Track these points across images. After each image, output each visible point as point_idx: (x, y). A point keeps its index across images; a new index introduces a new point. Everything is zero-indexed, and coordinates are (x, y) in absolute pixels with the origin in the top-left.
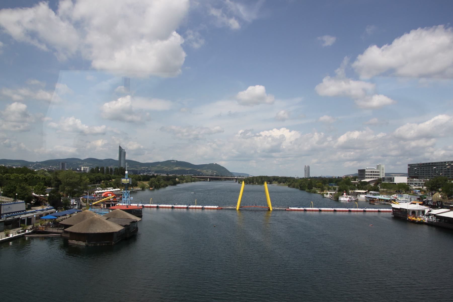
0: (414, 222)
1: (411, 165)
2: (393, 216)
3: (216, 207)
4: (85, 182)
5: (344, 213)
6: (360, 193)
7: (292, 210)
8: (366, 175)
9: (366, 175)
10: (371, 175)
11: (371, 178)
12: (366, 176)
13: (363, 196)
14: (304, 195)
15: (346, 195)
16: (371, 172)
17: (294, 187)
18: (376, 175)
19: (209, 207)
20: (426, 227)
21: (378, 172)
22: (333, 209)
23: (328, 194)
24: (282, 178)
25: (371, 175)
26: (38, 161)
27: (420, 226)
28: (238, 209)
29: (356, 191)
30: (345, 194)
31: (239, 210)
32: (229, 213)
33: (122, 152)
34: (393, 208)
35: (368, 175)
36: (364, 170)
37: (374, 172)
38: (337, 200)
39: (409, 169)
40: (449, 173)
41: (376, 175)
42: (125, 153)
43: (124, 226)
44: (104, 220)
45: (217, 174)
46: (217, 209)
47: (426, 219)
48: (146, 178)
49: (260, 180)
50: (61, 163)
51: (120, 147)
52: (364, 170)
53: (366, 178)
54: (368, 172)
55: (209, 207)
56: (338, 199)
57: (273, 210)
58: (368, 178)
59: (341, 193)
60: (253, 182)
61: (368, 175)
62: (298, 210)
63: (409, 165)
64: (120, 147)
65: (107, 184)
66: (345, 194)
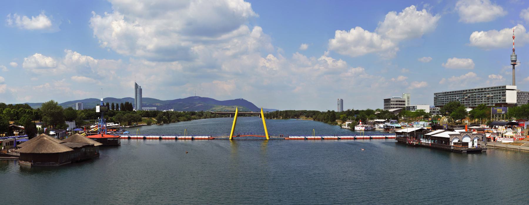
2: (397, 141)
3: (207, 137)
4: (80, 116)
5: (349, 140)
6: (379, 122)
7: (291, 139)
10: (397, 104)
11: (397, 108)
13: (382, 125)
14: (327, 126)
15: (362, 124)
16: (397, 101)
17: (319, 120)
18: (401, 105)
19: (200, 137)
22: (336, 137)
23: (346, 125)
24: (310, 112)
25: (397, 104)
28: (230, 138)
29: (375, 120)
30: (361, 123)
32: (222, 144)
33: (138, 89)
35: (394, 104)
38: (353, 129)
39: (435, 98)
41: (401, 105)
42: (141, 90)
44: (56, 144)
45: (248, 110)
46: (208, 139)
48: (154, 114)
49: (284, 115)
50: (77, 104)
51: (136, 84)
54: (394, 101)
55: (200, 137)
56: (354, 128)
59: (358, 123)
60: (277, 117)
61: (394, 104)
62: (298, 139)
64: (136, 84)
65: (107, 119)
66: (361, 123)
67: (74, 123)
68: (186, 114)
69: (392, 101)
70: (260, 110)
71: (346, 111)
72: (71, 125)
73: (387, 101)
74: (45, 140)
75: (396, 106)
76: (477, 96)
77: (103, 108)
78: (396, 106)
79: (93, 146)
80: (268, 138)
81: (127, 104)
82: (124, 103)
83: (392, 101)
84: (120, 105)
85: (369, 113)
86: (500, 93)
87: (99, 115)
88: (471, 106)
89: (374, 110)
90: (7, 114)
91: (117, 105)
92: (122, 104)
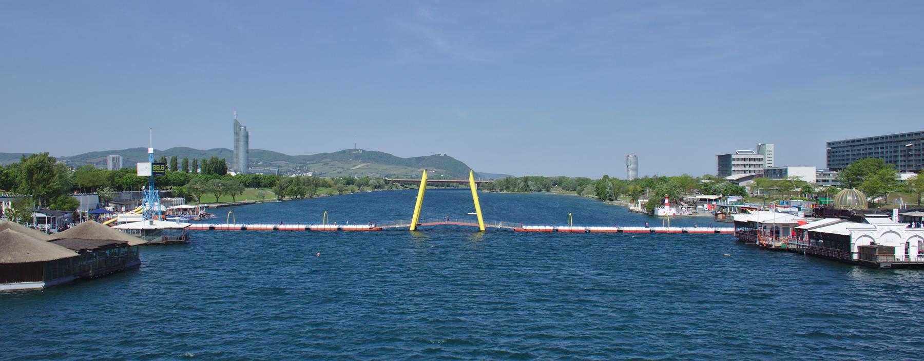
0: (768, 248)
1: (833, 143)
8: (734, 166)
9: (734, 166)
10: (745, 166)
11: (745, 172)
12: (733, 169)
16: (745, 160)
20: (793, 260)
21: (759, 160)
25: (745, 166)
26: (66, 156)
27: (779, 254)
28: (412, 228)
31: (416, 229)
34: (738, 224)
35: (738, 166)
36: (730, 156)
37: (750, 160)
39: (829, 152)
40: (911, 158)
43: (81, 252)
47: (795, 244)
51: (236, 124)
52: (730, 156)
53: (734, 172)
54: (738, 159)
56: (653, 212)
57: (487, 231)
58: (738, 172)
61: (738, 166)
63: (829, 144)
64: (236, 124)
67: (97, 197)
68: (337, 182)
69: (734, 159)
70: (469, 169)
71: (642, 180)
72: (85, 202)
73: (725, 162)
74: (8, 235)
75: (743, 169)
76: (850, 153)
77: (157, 167)
78: (743, 169)
79: (125, 244)
80: (482, 228)
81: (214, 161)
82: (208, 160)
83: (734, 159)
84: (199, 163)
85: (687, 184)
86: (882, 148)
87: (146, 181)
88: (914, 168)
89: (701, 177)
90: (204, 171)
91: (195, 162)
92: (204, 161)
